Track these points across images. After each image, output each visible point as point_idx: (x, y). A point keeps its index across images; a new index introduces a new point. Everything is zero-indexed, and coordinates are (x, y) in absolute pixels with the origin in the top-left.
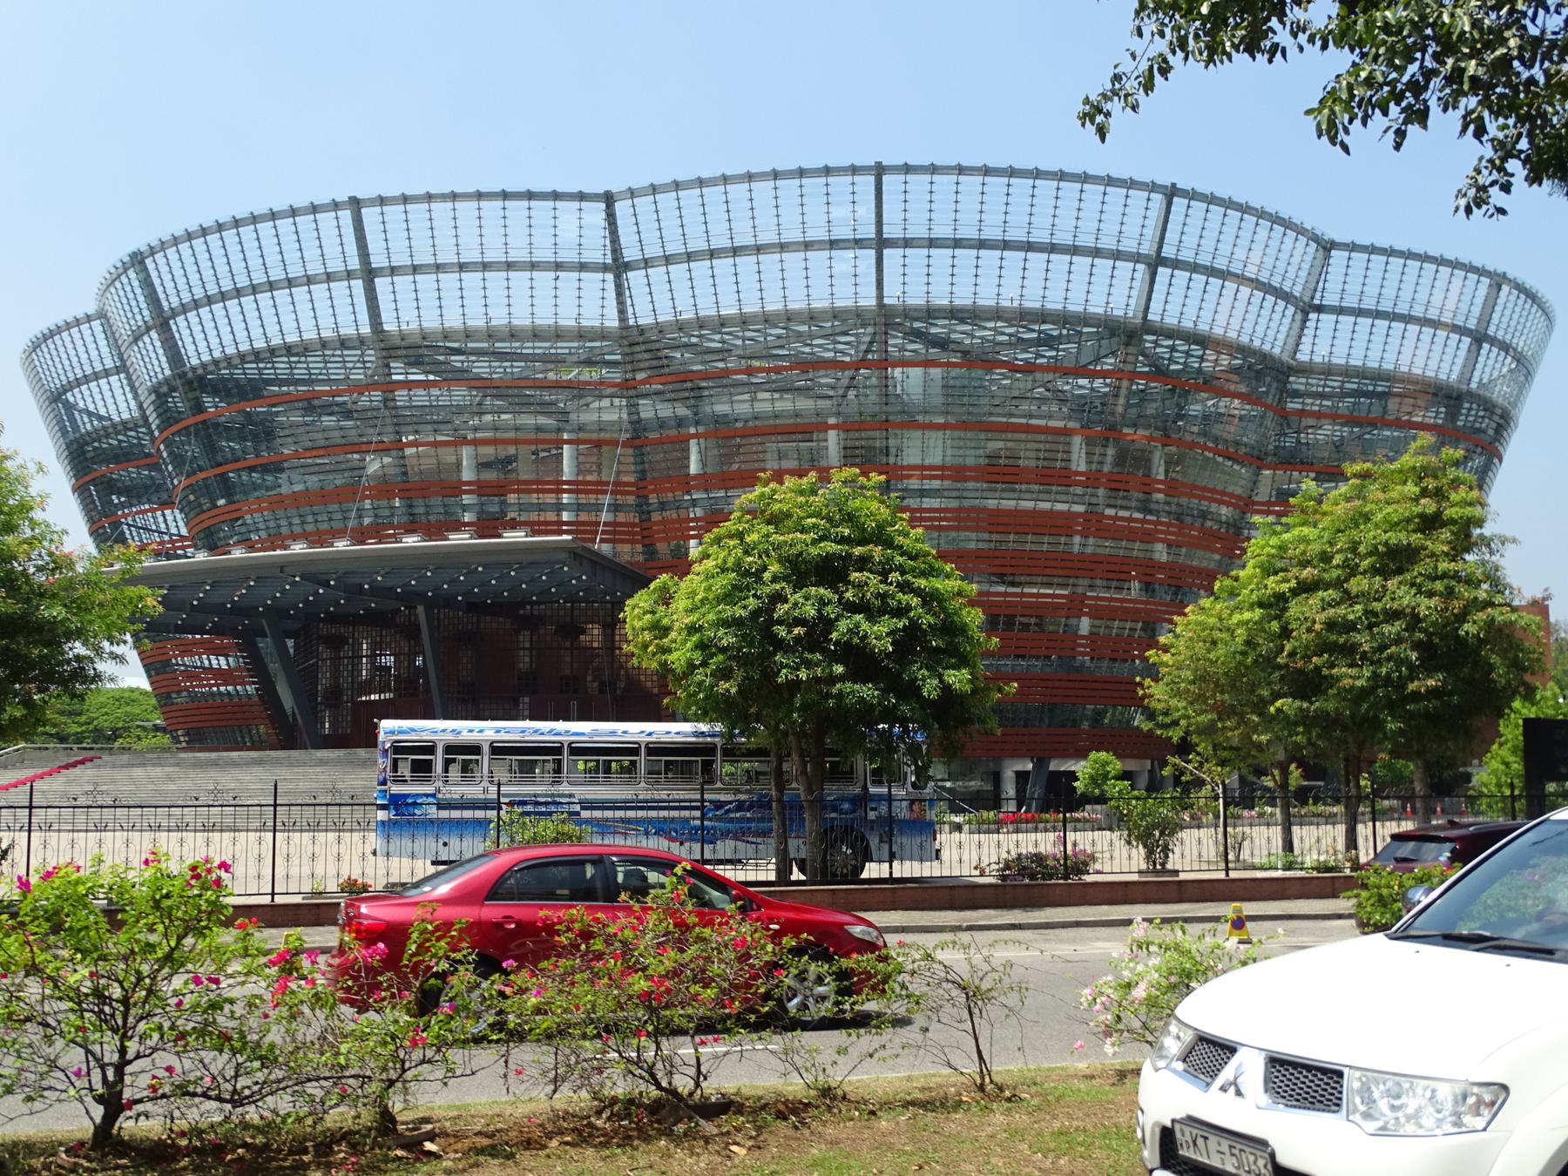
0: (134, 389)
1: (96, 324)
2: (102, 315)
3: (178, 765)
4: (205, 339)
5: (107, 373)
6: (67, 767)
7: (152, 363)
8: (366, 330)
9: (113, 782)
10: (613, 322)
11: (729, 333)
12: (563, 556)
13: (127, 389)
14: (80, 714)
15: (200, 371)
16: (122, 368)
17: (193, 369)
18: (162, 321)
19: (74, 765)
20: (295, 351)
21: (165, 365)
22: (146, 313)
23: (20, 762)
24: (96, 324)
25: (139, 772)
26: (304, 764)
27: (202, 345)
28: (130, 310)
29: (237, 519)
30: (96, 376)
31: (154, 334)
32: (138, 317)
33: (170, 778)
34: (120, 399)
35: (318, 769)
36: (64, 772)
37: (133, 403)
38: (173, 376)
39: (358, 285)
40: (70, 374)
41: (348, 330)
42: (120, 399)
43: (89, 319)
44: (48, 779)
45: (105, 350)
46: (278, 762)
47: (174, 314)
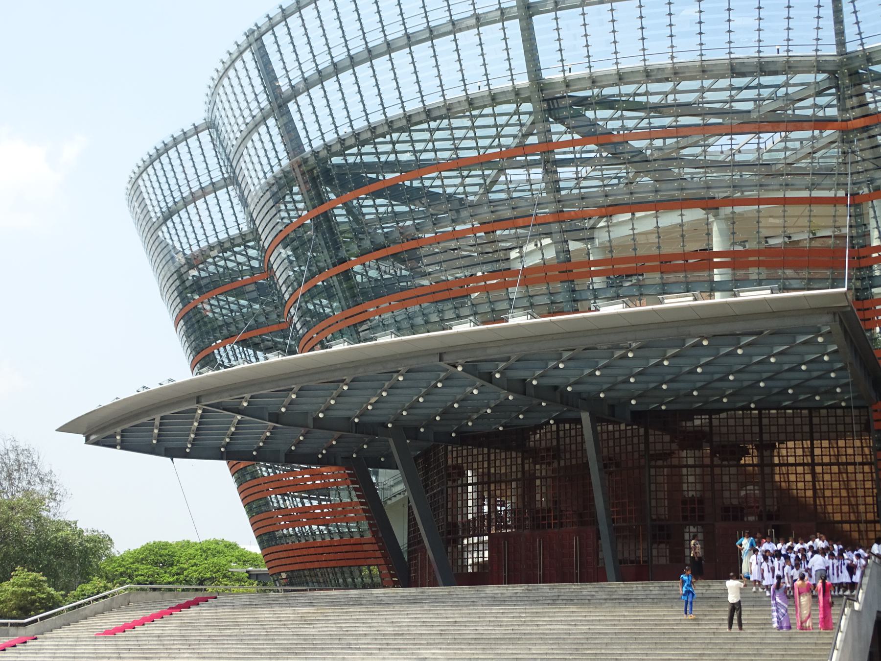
0: (245, 204)
1: (204, 136)
2: (211, 125)
3: (311, 604)
4: (323, 120)
5: (215, 187)
6: (179, 607)
7: (265, 158)
8: (523, 81)
9: (237, 624)
10: (830, 50)
11: (822, 157)
12: (826, 324)
13: (236, 201)
14: (172, 565)
15: (323, 154)
16: (232, 180)
17: (315, 153)
18: (279, 104)
19: (187, 605)
20: (435, 114)
21: (283, 155)
22: (263, 97)
23: (126, 603)
24: (204, 136)
25: (265, 614)
26: (474, 603)
27: (326, 122)
28: (248, 92)
29: (362, 323)
30: (203, 192)
31: (271, 122)
32: (254, 105)
33: (305, 621)
34: (228, 213)
35: (495, 609)
36: (176, 614)
37: (241, 216)
38: (291, 165)
39: (514, 27)
40: (177, 194)
41: (501, 84)
42: (228, 213)
43: (197, 130)
44: (158, 621)
45: (212, 162)
46: (457, 604)
47: (295, 93)
